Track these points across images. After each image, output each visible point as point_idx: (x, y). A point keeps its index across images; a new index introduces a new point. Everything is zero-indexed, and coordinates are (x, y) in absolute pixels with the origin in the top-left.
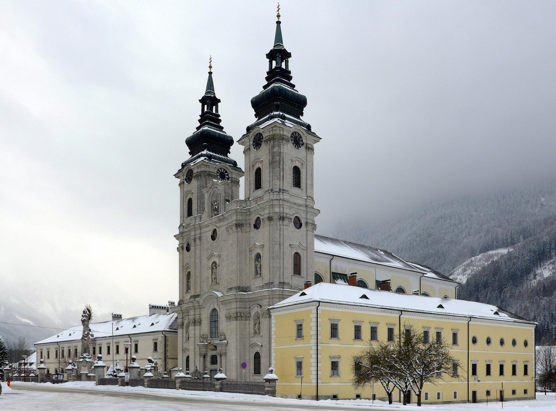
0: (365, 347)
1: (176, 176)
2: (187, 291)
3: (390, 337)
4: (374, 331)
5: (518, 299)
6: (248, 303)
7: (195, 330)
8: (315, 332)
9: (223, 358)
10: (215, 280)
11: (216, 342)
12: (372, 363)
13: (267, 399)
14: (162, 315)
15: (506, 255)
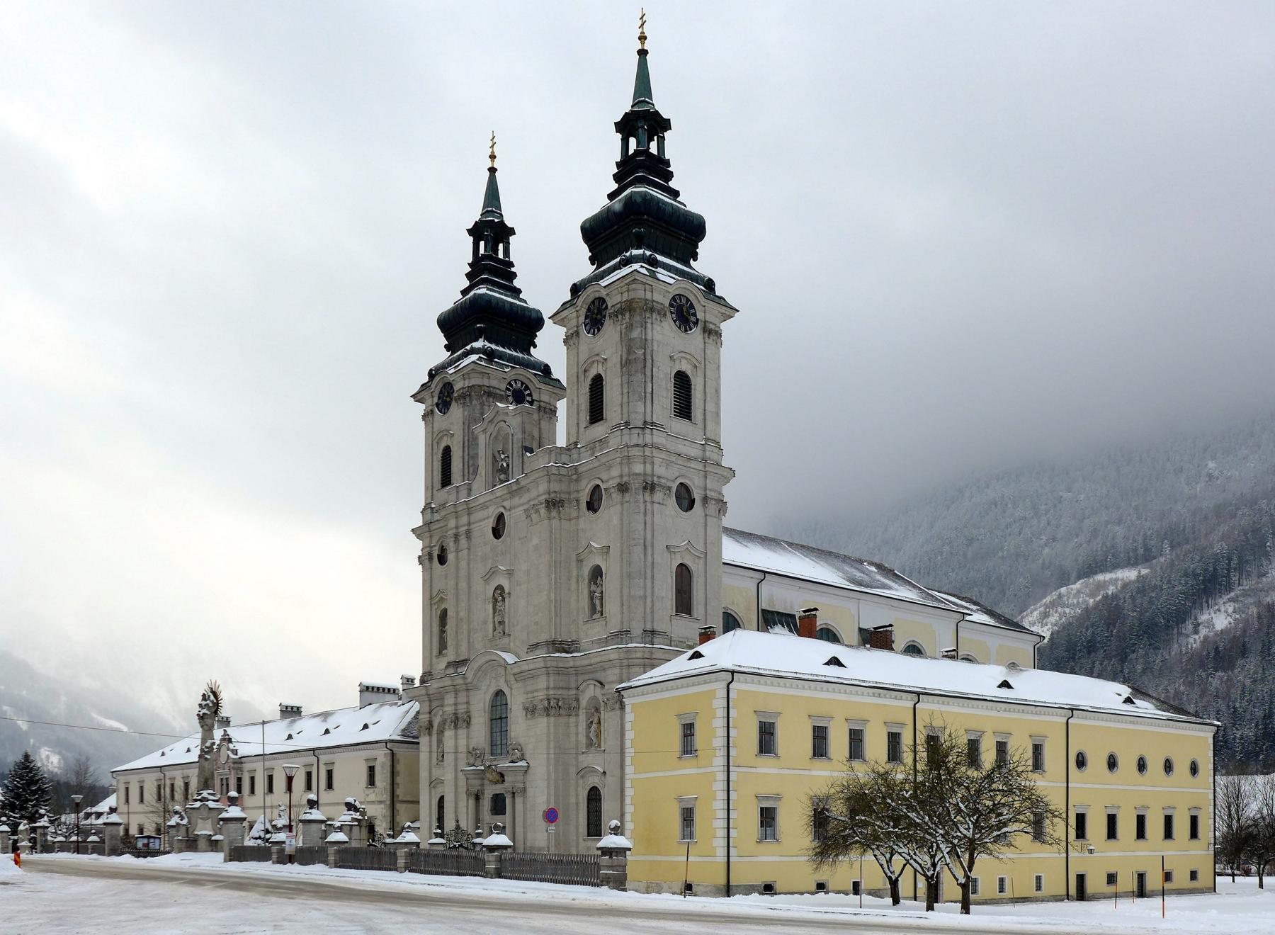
0: (835, 774)
1: (417, 397)
2: (440, 652)
3: (894, 753)
4: (856, 738)
5: (1161, 675)
6: (573, 678)
7: (456, 739)
8: (723, 742)
9: (519, 800)
10: (501, 628)
11: (504, 764)
12: (853, 812)
13: (606, 896)
14: (386, 707)
15: (1134, 582)
